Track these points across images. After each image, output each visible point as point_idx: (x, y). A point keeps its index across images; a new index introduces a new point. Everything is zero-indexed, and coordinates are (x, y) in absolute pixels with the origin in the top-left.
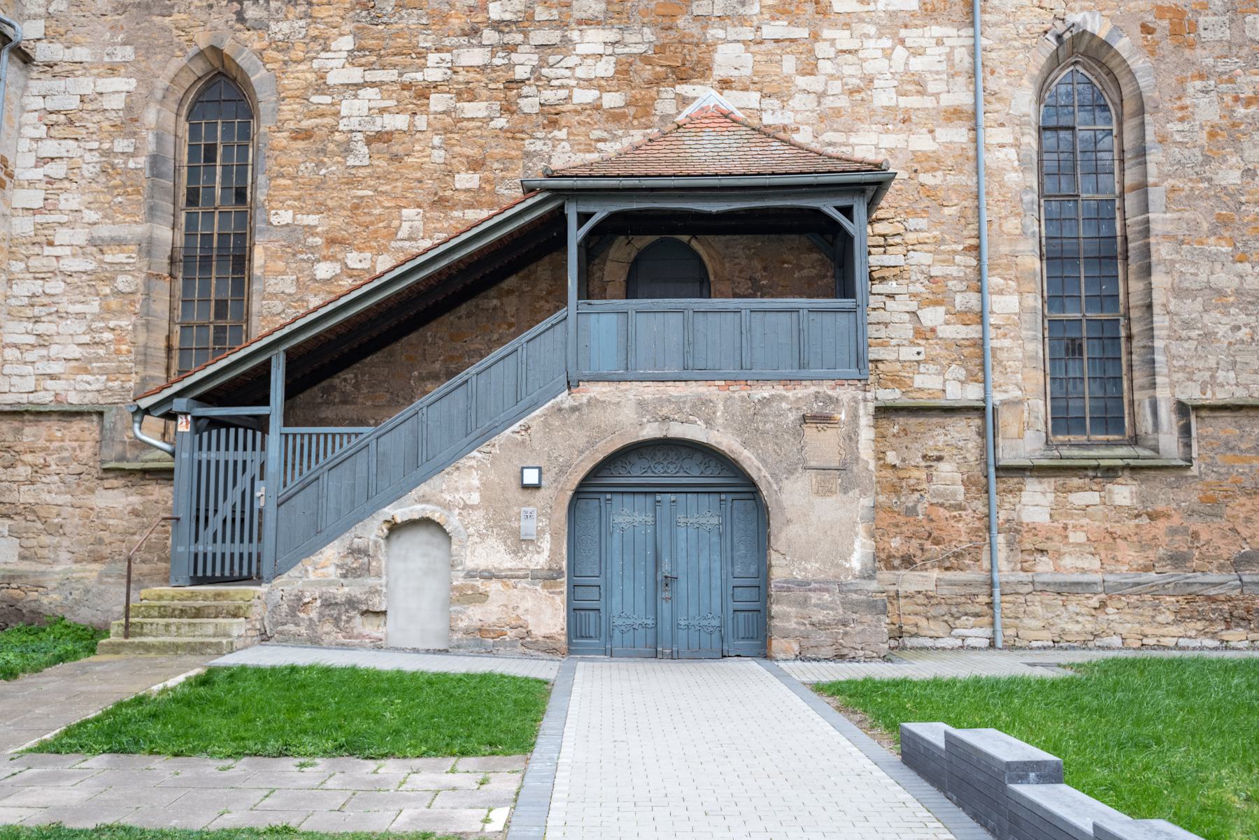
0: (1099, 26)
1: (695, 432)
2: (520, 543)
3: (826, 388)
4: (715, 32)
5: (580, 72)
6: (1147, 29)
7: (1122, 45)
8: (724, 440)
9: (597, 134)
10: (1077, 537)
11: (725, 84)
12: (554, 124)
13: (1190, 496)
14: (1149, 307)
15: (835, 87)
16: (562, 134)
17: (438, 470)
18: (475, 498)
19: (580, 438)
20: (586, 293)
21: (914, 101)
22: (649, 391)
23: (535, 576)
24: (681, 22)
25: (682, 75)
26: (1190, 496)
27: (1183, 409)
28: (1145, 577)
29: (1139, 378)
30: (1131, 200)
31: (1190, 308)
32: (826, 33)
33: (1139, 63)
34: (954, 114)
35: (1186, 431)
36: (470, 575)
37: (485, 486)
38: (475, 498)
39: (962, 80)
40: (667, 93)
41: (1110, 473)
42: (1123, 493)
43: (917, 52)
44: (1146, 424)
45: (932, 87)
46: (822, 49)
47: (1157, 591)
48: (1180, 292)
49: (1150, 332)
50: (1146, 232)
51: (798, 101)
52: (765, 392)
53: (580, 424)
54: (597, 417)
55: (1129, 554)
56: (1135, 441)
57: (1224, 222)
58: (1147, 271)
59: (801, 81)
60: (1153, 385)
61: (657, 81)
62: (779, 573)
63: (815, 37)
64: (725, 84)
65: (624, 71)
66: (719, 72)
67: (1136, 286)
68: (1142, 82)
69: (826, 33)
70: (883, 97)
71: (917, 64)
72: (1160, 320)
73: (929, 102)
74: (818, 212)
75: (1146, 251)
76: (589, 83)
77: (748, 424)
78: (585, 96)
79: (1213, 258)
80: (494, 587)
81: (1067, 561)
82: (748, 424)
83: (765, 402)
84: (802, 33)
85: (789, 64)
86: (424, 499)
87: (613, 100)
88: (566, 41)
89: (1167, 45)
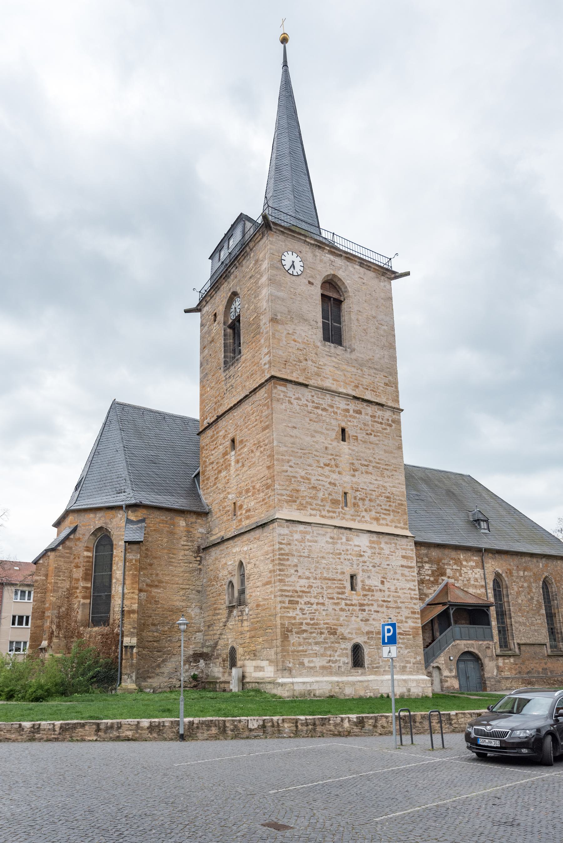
0: (500, 572)
1: (471, 650)
2: (451, 671)
3: (488, 642)
4: (446, 567)
5: (426, 573)
6: (507, 573)
7: (503, 575)
8: (476, 651)
9: (430, 586)
10: (507, 668)
11: (449, 577)
12: (423, 583)
13: (520, 661)
14: (512, 625)
15: (465, 579)
16: (424, 585)
17: (437, 657)
18: (443, 662)
19: (457, 651)
20: (456, 623)
21: (476, 583)
22: (465, 642)
23: (453, 677)
24: (440, 564)
25: (442, 576)
26: (520, 661)
27: (519, 644)
28: (517, 676)
29: (510, 638)
30: (506, 604)
31: (517, 625)
32: (463, 569)
33: (506, 579)
34: (482, 586)
35: (519, 648)
36: (445, 677)
37: (445, 660)
38: (443, 662)
39: (483, 580)
40: (440, 578)
41: (510, 656)
42: (512, 660)
43: (476, 574)
44: (512, 647)
45: (479, 581)
46: (462, 572)
47: (518, 678)
48: (516, 622)
49: (512, 630)
50: (510, 610)
51: (460, 582)
52: (480, 643)
53: (457, 648)
54: (459, 647)
55: (514, 672)
56: (510, 650)
57: (520, 610)
58: (510, 618)
59: (460, 578)
60: (513, 640)
61: (438, 576)
62: (486, 675)
63: (461, 569)
64: (449, 577)
65: (433, 572)
66: (448, 575)
67: (508, 620)
68: (507, 582)
69: (463, 569)
70: (472, 582)
71: (476, 576)
72: (514, 628)
73: (478, 584)
74: (483, 610)
75: (510, 614)
76: (428, 575)
77: (479, 647)
78: (427, 578)
79: (519, 616)
80: (448, 679)
81: (506, 673)
82: (479, 647)
83: (481, 644)
84: (459, 568)
85: (458, 574)
86: (437, 662)
87: (432, 579)
88: (423, 566)
89: (509, 576)
